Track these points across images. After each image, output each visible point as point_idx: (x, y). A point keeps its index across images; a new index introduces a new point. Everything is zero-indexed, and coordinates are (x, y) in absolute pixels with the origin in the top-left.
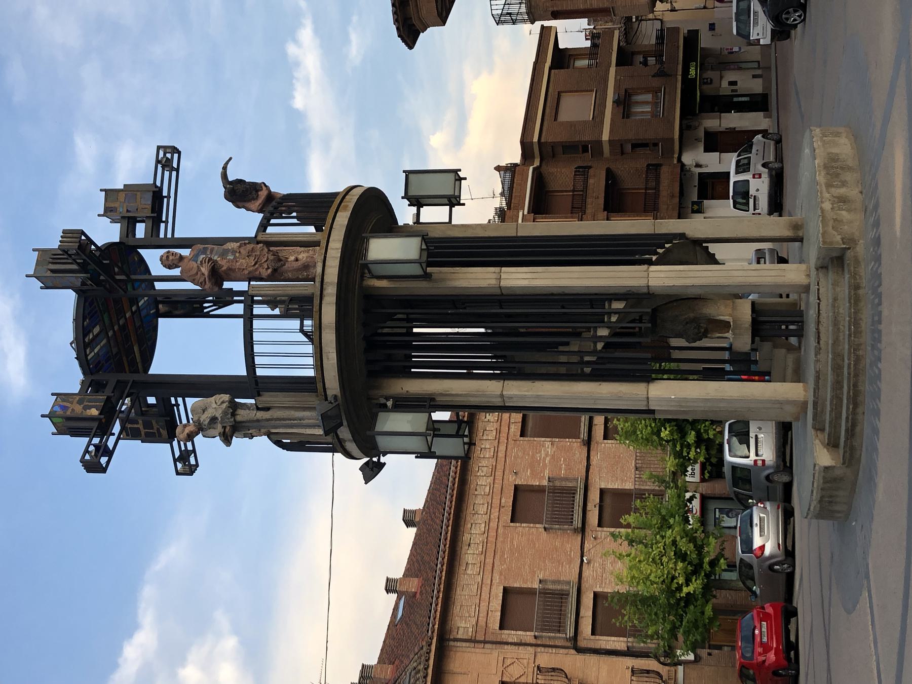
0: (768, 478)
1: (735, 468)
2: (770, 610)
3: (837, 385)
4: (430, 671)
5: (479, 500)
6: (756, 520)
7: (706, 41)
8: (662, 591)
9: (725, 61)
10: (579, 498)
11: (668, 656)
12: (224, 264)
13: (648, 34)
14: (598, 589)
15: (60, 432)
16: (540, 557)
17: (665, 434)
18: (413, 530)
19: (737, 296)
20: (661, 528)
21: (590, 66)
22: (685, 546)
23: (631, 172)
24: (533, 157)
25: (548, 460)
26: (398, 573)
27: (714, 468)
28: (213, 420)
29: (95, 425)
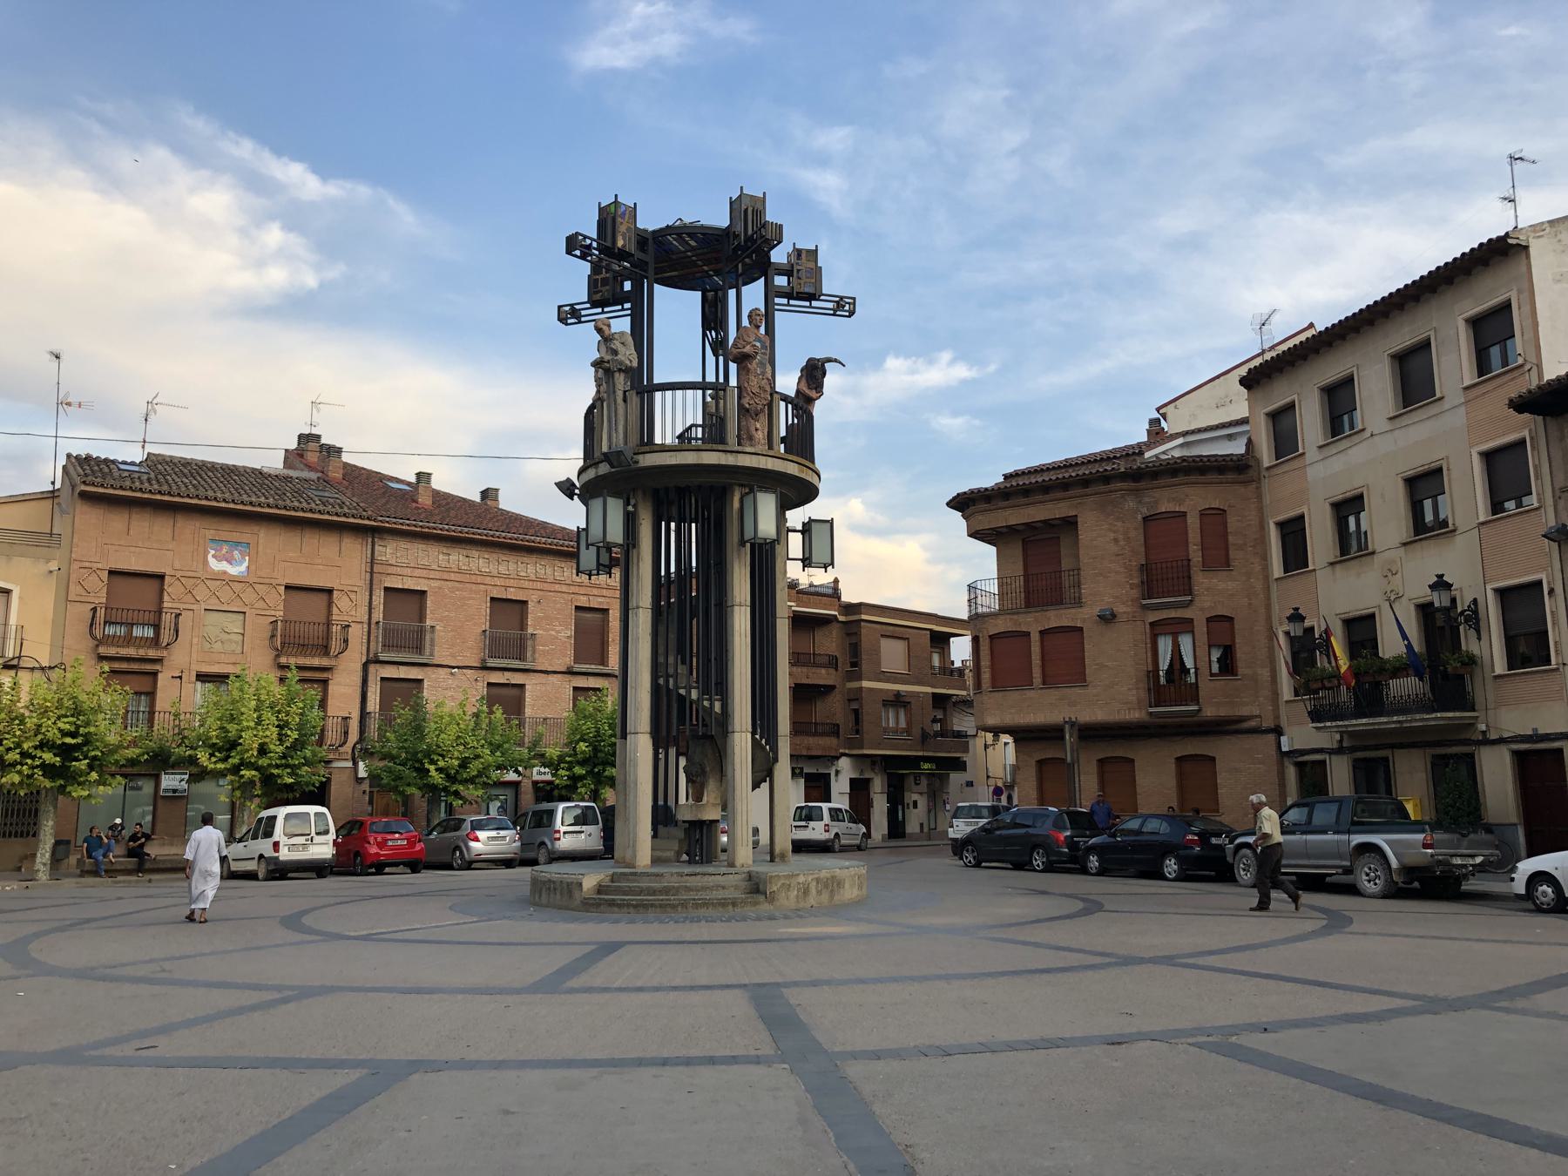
0: (543, 843)
1: (551, 814)
2: (418, 848)
3: (654, 892)
4: (343, 519)
5: (512, 566)
6: (503, 833)
7: (956, 778)
8: (429, 746)
9: (936, 797)
10: (516, 664)
11: (363, 751)
12: (753, 365)
13: (963, 723)
14: (426, 683)
15: (601, 210)
16: (458, 626)
17: (582, 746)
18: (477, 499)
19: (724, 809)
20: (491, 744)
21: (932, 667)
22: (474, 768)
23: (833, 709)
24: (846, 615)
25: (553, 635)
26: (436, 484)
27: (547, 793)
28: (615, 352)
29: (609, 244)
